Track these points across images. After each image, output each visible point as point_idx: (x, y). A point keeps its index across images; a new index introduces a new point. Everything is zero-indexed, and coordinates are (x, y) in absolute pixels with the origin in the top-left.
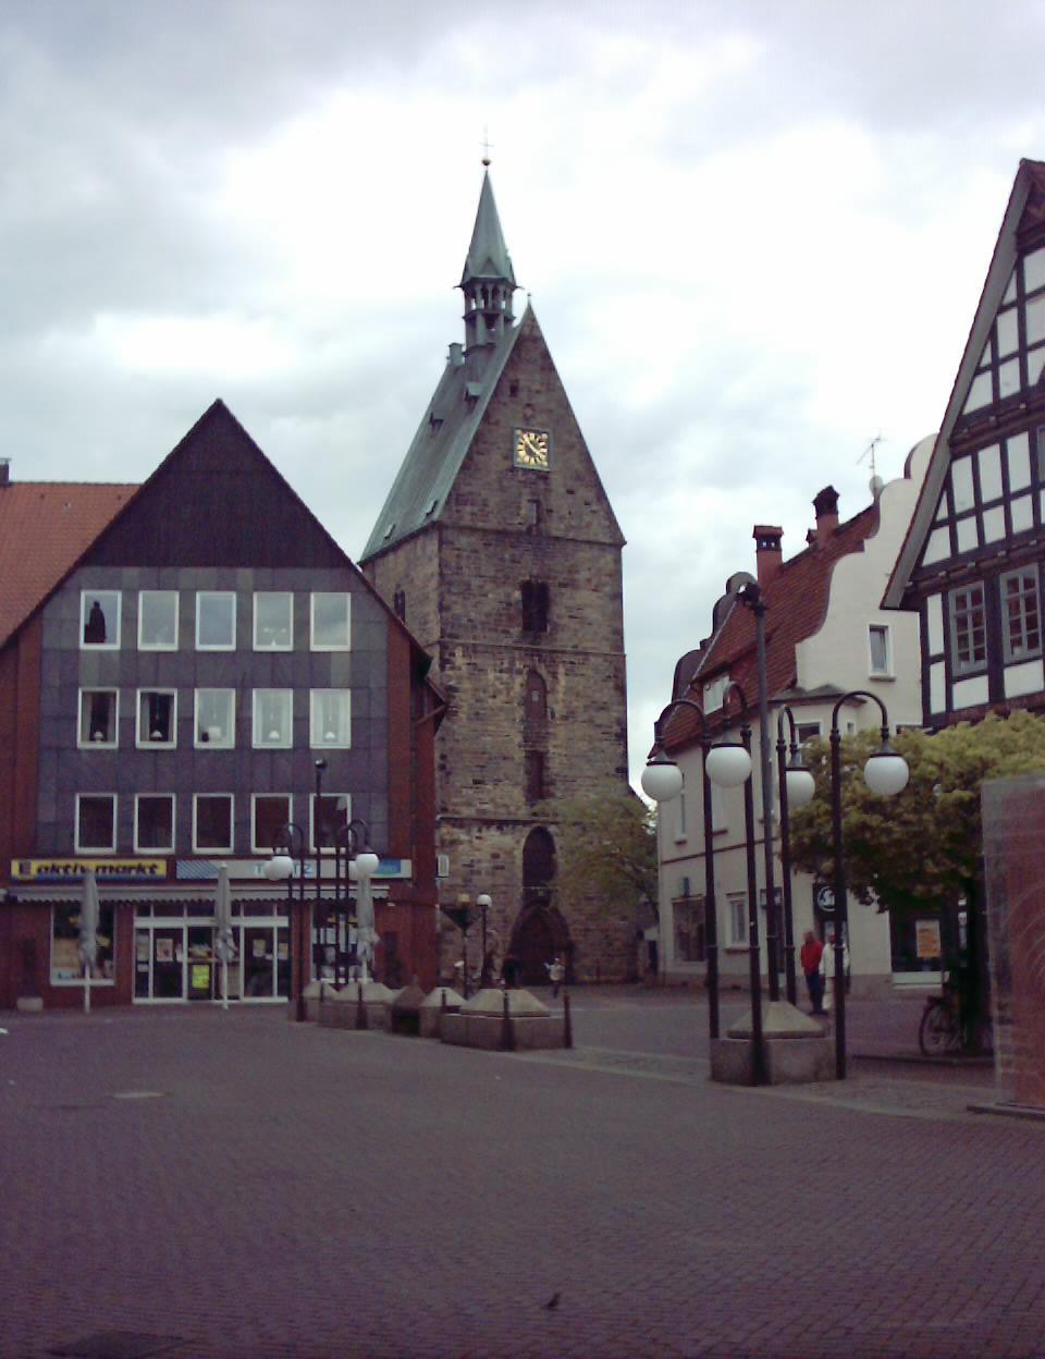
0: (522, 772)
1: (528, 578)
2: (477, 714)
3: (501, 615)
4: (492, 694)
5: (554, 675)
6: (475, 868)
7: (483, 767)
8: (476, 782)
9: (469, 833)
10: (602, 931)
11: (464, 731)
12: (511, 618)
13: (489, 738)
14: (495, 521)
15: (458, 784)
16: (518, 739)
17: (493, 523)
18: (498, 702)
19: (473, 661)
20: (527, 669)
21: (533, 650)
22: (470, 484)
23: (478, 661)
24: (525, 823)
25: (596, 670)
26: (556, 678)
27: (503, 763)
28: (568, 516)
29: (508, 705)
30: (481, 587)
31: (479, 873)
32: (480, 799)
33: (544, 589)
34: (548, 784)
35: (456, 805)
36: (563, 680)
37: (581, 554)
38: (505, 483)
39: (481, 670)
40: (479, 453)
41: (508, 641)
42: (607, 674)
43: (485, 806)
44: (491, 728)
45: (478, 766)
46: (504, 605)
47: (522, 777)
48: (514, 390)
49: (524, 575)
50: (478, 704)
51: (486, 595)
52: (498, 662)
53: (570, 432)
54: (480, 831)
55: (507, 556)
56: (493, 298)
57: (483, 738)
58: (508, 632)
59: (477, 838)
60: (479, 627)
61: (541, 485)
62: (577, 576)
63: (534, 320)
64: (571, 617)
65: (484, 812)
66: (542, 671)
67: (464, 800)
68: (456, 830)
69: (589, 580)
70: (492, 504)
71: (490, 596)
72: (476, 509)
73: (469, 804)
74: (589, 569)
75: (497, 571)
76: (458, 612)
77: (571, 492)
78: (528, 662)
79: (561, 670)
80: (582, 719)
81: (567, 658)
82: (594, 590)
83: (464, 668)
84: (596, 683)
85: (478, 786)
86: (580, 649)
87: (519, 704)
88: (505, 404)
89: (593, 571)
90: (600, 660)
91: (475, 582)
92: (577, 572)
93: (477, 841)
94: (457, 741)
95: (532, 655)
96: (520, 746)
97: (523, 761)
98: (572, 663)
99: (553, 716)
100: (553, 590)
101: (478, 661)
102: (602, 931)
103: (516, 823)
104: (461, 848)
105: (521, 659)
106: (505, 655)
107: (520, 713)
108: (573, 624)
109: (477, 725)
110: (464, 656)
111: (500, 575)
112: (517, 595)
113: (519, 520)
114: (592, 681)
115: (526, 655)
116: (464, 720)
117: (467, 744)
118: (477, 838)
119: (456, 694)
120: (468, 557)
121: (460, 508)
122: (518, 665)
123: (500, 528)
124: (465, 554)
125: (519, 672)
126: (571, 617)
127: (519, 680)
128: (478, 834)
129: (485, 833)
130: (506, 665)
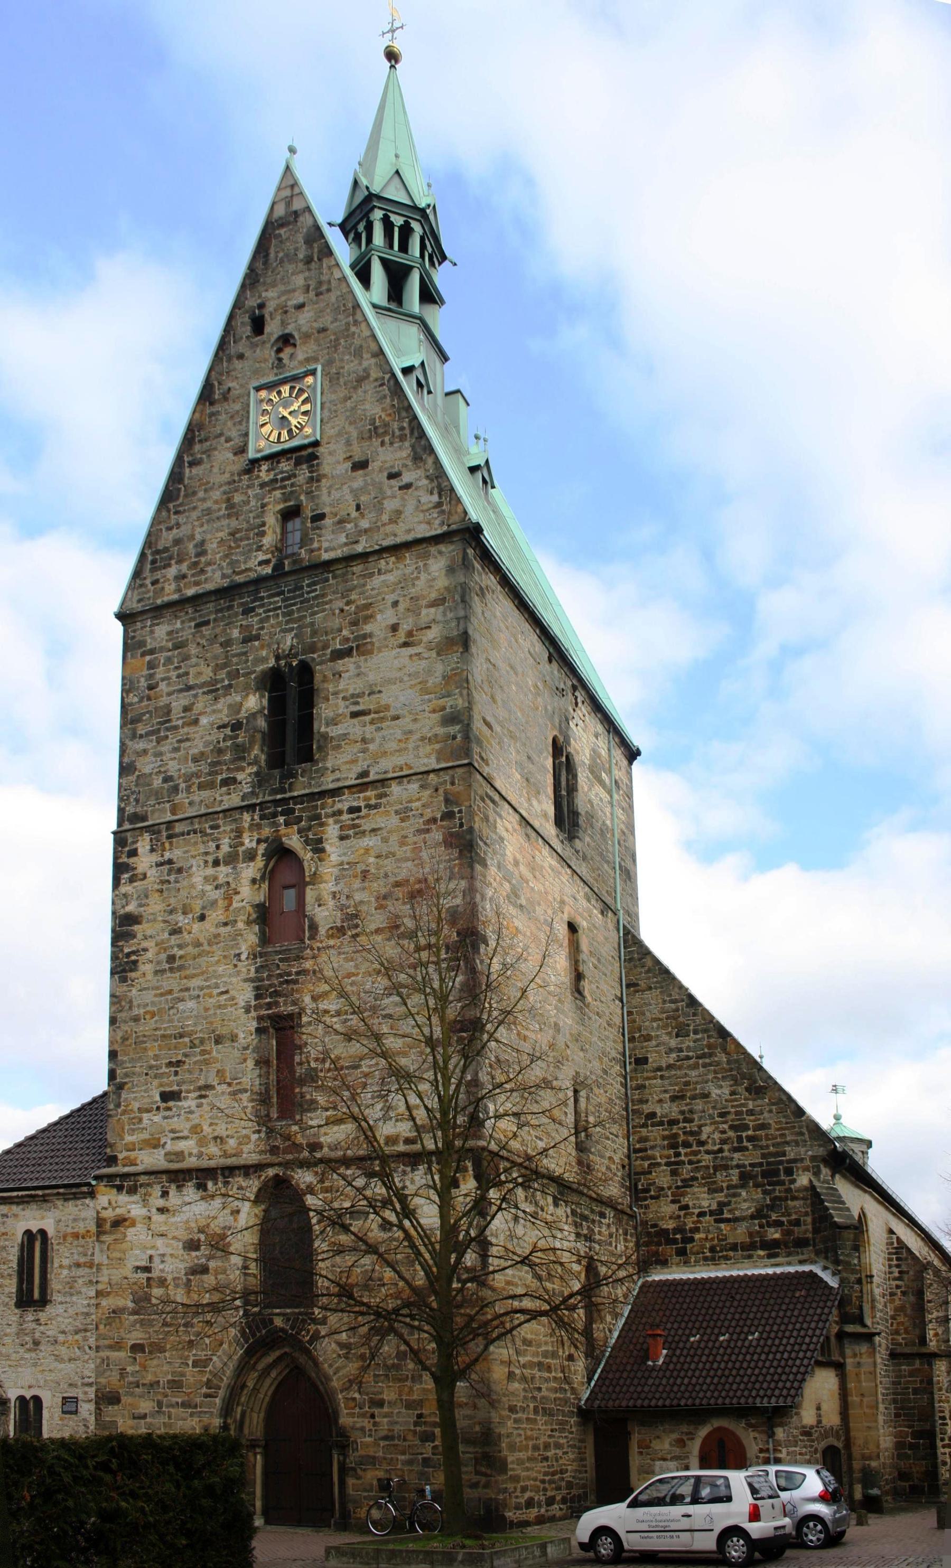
0: (250, 1063)
1: (272, 663)
2: (171, 959)
3: (220, 751)
4: (198, 912)
5: (318, 847)
6: (155, 1274)
7: (179, 1063)
8: (167, 1097)
9: (145, 1202)
10: (409, 1405)
11: (149, 997)
12: (240, 752)
13: (191, 1004)
14: (218, 574)
15: (136, 1105)
16: (245, 994)
17: (215, 579)
18: (209, 927)
19: (167, 855)
20: (263, 846)
21: (276, 803)
22: (178, 525)
23: (175, 854)
24: (247, 1170)
25: (404, 814)
26: (323, 850)
27: (216, 1051)
28: (354, 514)
29: (229, 928)
30: (186, 709)
31: (162, 1282)
32: (173, 1131)
33: (306, 671)
34: (302, 1082)
35: (131, 1148)
36: (334, 850)
37: (377, 581)
38: (238, 498)
39: (180, 871)
40: (192, 464)
41: (234, 800)
42: (428, 814)
43: (182, 1145)
44: (195, 983)
45: (170, 1064)
46: (228, 731)
47: (250, 1076)
48: (258, 325)
49: (264, 660)
50: (174, 940)
51: (196, 722)
52: (212, 845)
53: (358, 353)
54: (165, 1194)
55: (236, 633)
56: (267, 1090)
57: (181, 1006)
58: (234, 781)
59: (161, 1210)
60: (183, 786)
61: (303, 473)
62: (368, 628)
63: (294, 185)
64: (355, 715)
65: (180, 1155)
66: (294, 841)
67: (145, 1136)
68: (123, 1198)
69: (394, 628)
70: (212, 546)
71: (204, 721)
72: (184, 567)
73: (154, 1144)
74: (395, 604)
75: (215, 671)
76: (147, 770)
77: (360, 465)
78: (267, 832)
79: (332, 831)
80: (373, 927)
81: (346, 802)
82: (406, 645)
83: (152, 873)
84: (403, 842)
85: (171, 1104)
86: (372, 777)
87: (248, 923)
88: (241, 357)
89: (401, 607)
90: (409, 864)
91: (178, 703)
92: (369, 618)
93: (157, 1218)
94: (136, 1019)
95: (275, 815)
96: (248, 1011)
97: (253, 1039)
98: (352, 810)
99: (314, 927)
100: (320, 671)
101: (175, 854)
102: (409, 1405)
103: (229, 1171)
104: (131, 1232)
105: (254, 827)
106: (226, 827)
107: (250, 938)
108: (354, 728)
109: (171, 982)
110: (152, 850)
111: (222, 674)
112: (253, 702)
113: (262, 557)
114: (394, 838)
115: (262, 817)
116: (150, 976)
117: (152, 1023)
118: (161, 1210)
119: (136, 928)
120: (169, 660)
121: (158, 575)
122: (248, 842)
123: (225, 583)
124: (162, 657)
125: (251, 856)
126: (355, 715)
127: (250, 871)
128: (161, 1203)
129: (174, 1199)
130: (225, 848)
